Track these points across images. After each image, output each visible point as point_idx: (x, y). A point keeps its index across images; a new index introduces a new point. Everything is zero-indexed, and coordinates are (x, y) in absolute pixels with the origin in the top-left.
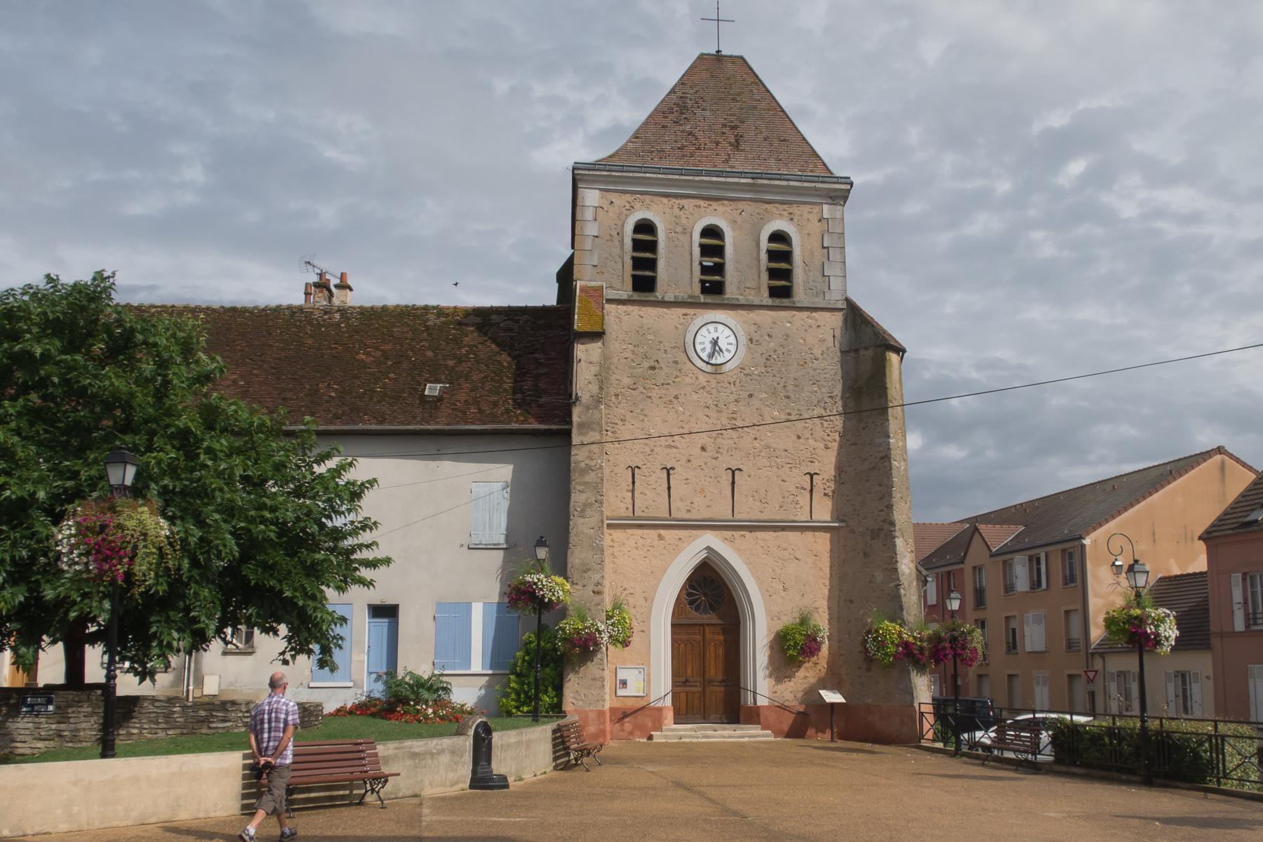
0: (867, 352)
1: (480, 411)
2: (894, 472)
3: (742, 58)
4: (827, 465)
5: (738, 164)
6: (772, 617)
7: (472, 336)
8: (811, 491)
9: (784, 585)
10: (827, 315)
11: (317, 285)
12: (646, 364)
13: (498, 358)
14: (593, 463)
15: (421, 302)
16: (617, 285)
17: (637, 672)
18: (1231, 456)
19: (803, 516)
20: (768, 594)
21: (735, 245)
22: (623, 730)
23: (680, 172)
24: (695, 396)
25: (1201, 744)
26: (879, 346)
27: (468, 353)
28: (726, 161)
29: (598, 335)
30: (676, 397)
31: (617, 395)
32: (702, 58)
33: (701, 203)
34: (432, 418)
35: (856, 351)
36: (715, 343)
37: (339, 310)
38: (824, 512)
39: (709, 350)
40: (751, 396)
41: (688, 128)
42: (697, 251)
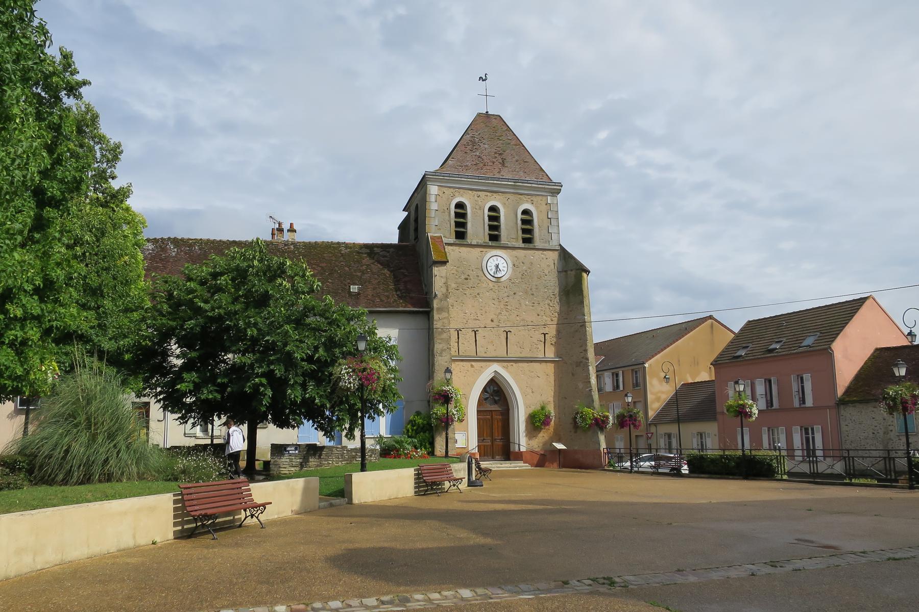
1: (381, 301)
4: (552, 331)
5: (506, 174)
6: (527, 406)
7: (367, 260)
9: (531, 391)
12: (463, 277)
19: (540, 355)
20: (525, 395)
23: (479, 178)
25: (772, 460)
28: (499, 172)
29: (444, 263)
32: (479, 115)
36: (497, 266)
38: (551, 354)
39: (494, 270)
42: (486, 218)
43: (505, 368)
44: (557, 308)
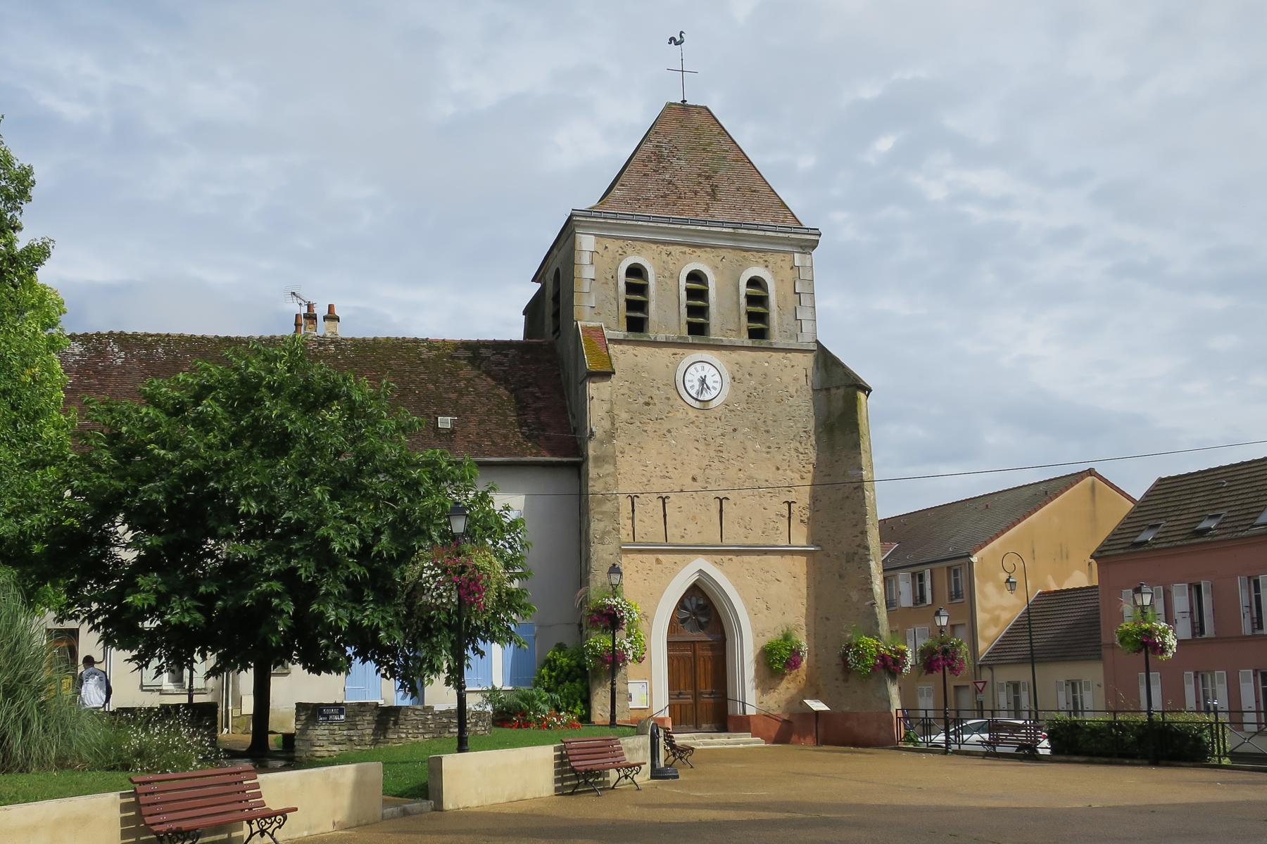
1: (494, 444)
4: (802, 497)
5: (718, 213)
6: (758, 634)
7: (467, 371)
9: (766, 605)
10: (800, 355)
11: (306, 316)
12: (641, 400)
13: (496, 391)
16: (614, 325)
18: (1101, 478)
19: (782, 541)
20: (753, 613)
21: (717, 289)
23: (668, 220)
24: (686, 431)
25: (1201, 731)
26: (850, 386)
27: (467, 387)
28: (706, 210)
29: (607, 375)
30: (669, 431)
32: (670, 106)
35: (828, 389)
36: (703, 381)
37: (332, 342)
38: (800, 538)
40: (735, 430)
43: (719, 564)
44: (813, 456)
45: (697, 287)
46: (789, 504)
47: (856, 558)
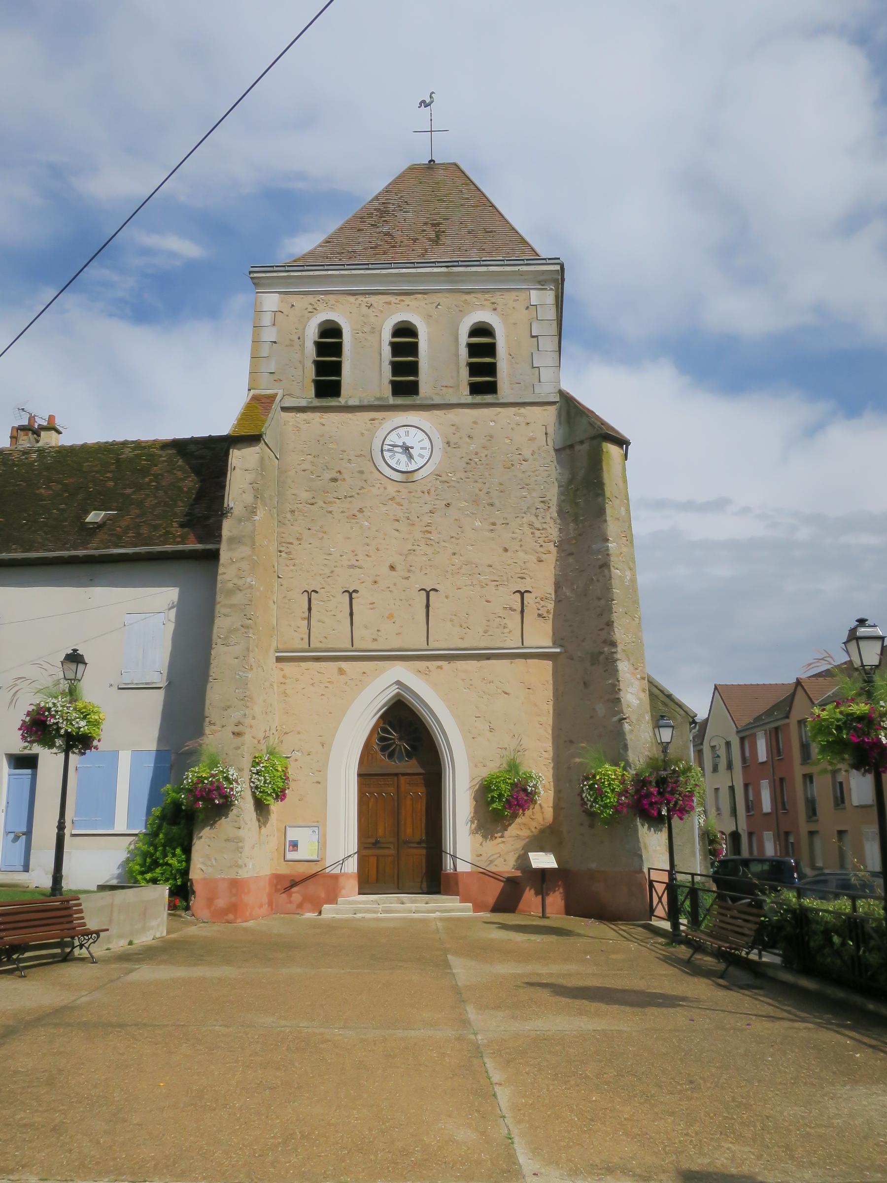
0: (586, 446)
2: (615, 582)
3: (455, 164)
8: (522, 612)
9: (493, 726)
12: (327, 476)
14: (240, 582)
15: (120, 439)
17: (309, 830)
19: (512, 642)
22: (290, 902)
24: (383, 509)
27: (151, 481)
30: (361, 511)
31: (293, 512)
33: (392, 299)
34: (84, 545)
38: (540, 636)
41: (385, 229)
43: (425, 673)
44: (554, 532)
45: (405, 340)
46: (523, 595)
47: (602, 658)
